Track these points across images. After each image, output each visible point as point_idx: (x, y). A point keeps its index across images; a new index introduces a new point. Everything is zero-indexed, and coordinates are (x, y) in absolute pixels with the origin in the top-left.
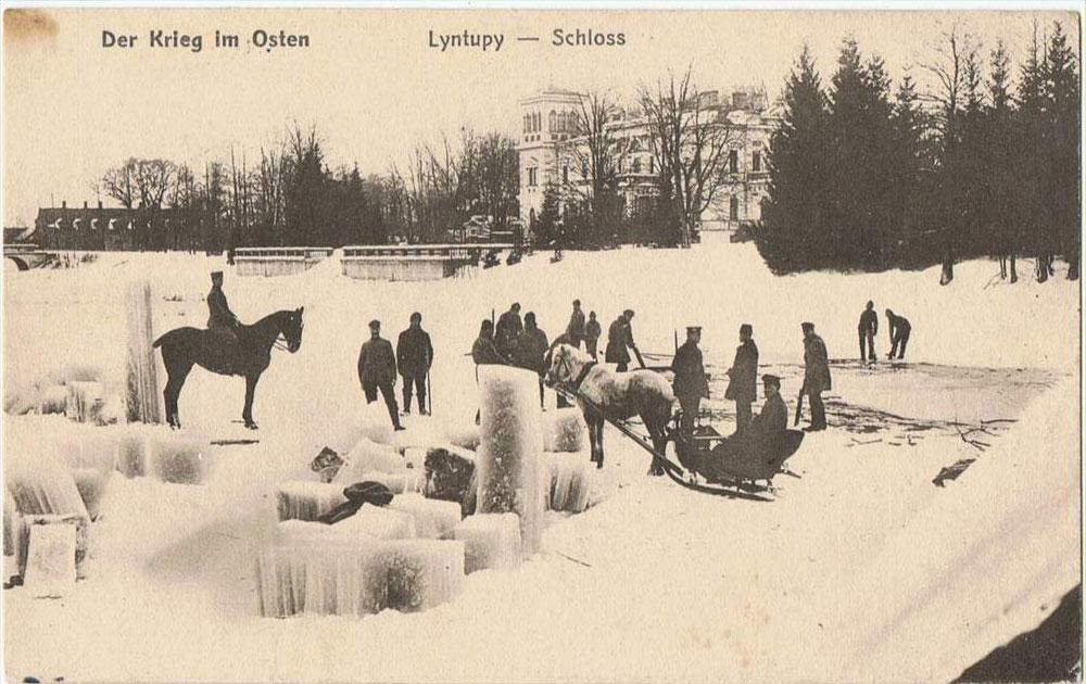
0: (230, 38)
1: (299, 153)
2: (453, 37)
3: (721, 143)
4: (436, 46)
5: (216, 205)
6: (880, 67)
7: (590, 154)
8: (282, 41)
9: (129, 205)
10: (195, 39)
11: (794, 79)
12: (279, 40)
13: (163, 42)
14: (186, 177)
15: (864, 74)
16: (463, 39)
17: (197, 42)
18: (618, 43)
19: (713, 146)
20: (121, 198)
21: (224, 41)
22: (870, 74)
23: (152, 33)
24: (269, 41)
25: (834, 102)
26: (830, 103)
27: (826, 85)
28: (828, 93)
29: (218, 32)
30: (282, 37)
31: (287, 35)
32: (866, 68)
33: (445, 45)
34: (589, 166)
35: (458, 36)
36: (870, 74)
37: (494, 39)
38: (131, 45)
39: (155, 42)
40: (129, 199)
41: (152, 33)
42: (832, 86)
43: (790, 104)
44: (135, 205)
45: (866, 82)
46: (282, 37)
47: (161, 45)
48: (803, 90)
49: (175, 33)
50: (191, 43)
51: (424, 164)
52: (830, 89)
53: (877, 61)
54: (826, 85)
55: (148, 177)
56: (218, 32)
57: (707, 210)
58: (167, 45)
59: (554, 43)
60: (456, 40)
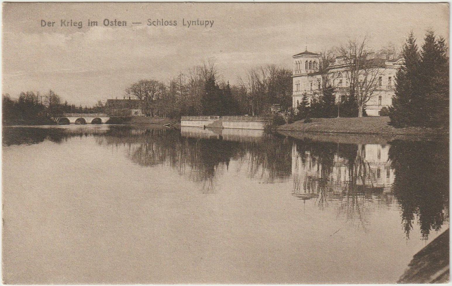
0: (94, 22)
1: (206, 78)
2: (193, 22)
3: (376, 74)
4: (186, 25)
5: (174, 99)
6: (443, 42)
7: (322, 79)
8: (116, 23)
9: (141, 99)
10: (79, 23)
11: (407, 47)
12: (114, 23)
13: (66, 24)
14: (162, 87)
15: (436, 45)
16: (197, 23)
17: (80, 24)
18: (111, 25)
19: (372, 75)
20: (138, 96)
21: (92, 24)
22: (439, 45)
23: (62, 20)
24: (110, 23)
25: (423, 57)
26: (422, 58)
27: (420, 49)
28: (420, 53)
29: (89, 20)
30: (115, 22)
31: (73, 22)
32: (437, 43)
33: (189, 25)
34: (321, 83)
35: (195, 22)
36: (439, 45)
37: (209, 22)
38: (53, 26)
39: (63, 25)
40: (141, 96)
41: (62, 20)
42: (422, 50)
43: (405, 58)
44: (143, 98)
45: (437, 49)
46: (115, 22)
47: (65, 26)
48: (410, 52)
49: (71, 20)
50: (77, 25)
51: (255, 83)
52: (421, 52)
53: (442, 40)
54: (420, 49)
55: (148, 88)
56: (89, 20)
57: (369, 101)
58: (68, 25)
59: (148, 25)
60: (194, 23)
